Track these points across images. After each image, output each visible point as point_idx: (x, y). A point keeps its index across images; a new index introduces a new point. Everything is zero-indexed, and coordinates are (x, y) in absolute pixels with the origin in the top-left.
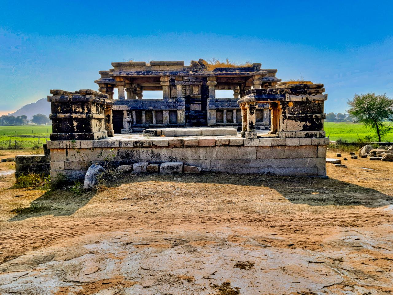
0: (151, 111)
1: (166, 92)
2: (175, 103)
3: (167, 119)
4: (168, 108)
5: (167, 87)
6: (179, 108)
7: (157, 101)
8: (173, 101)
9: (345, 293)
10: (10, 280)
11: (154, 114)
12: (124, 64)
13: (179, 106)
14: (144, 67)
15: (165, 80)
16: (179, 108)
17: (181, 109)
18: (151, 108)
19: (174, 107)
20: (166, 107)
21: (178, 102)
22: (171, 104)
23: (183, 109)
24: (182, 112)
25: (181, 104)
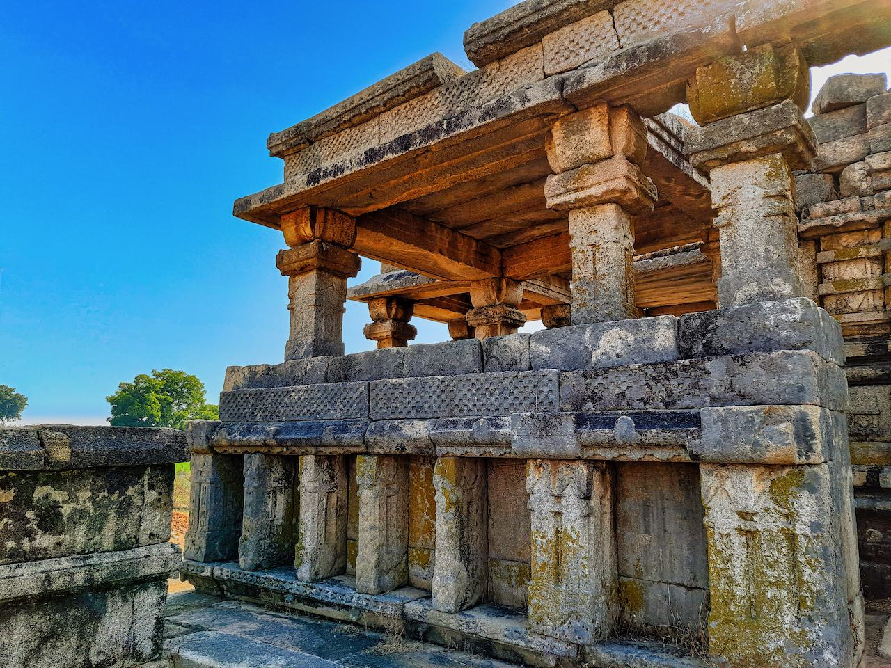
0: (426, 456)
1: (602, 268)
2: (661, 368)
3: (569, 565)
4: (567, 438)
5: (610, 210)
6: (708, 441)
7: (439, 346)
8: (641, 348)
9: (803, 388)
10: (766, 528)
11: (443, 489)
12: (320, 124)
13: (710, 413)
14: (435, 98)
15: (589, 151)
16: (708, 441)
17: (743, 449)
18: (420, 430)
19: (643, 420)
20: (546, 425)
21: (711, 352)
22: (617, 385)
23: (773, 451)
24: (778, 493)
25: (754, 376)
